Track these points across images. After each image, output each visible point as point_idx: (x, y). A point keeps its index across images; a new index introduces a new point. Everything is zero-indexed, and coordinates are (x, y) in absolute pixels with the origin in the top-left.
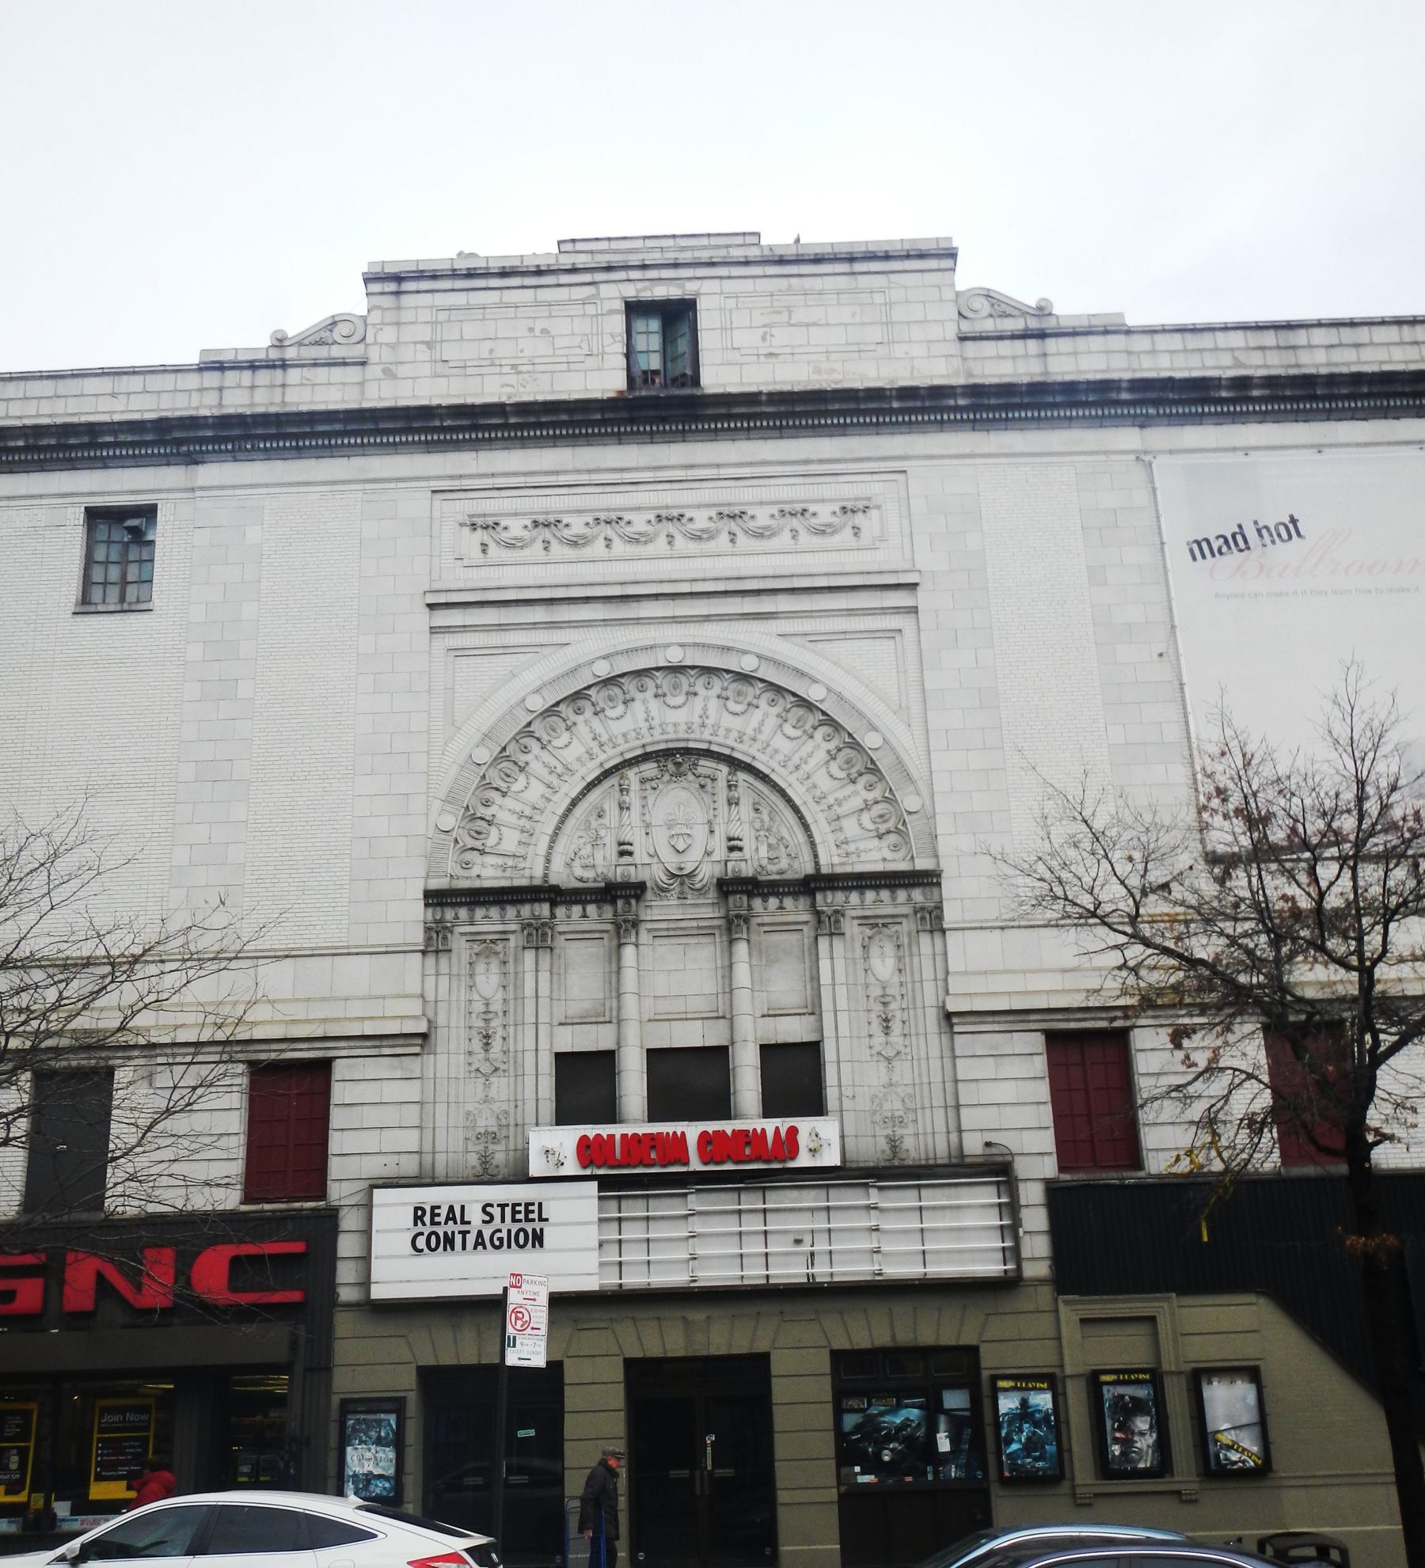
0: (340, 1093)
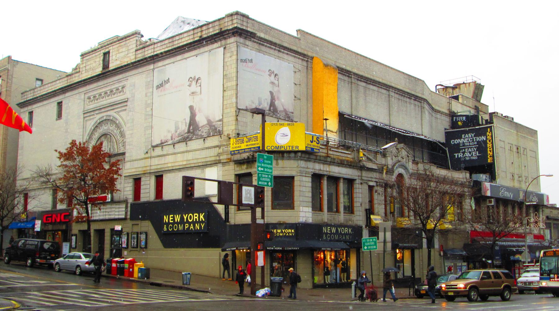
0: (142, 183)
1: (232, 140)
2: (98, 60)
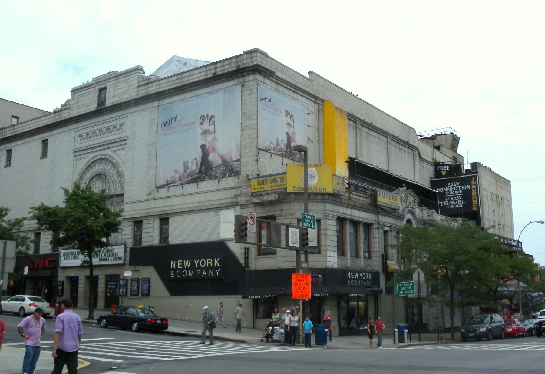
0: (144, 226)
1: (253, 181)
2: (91, 96)
